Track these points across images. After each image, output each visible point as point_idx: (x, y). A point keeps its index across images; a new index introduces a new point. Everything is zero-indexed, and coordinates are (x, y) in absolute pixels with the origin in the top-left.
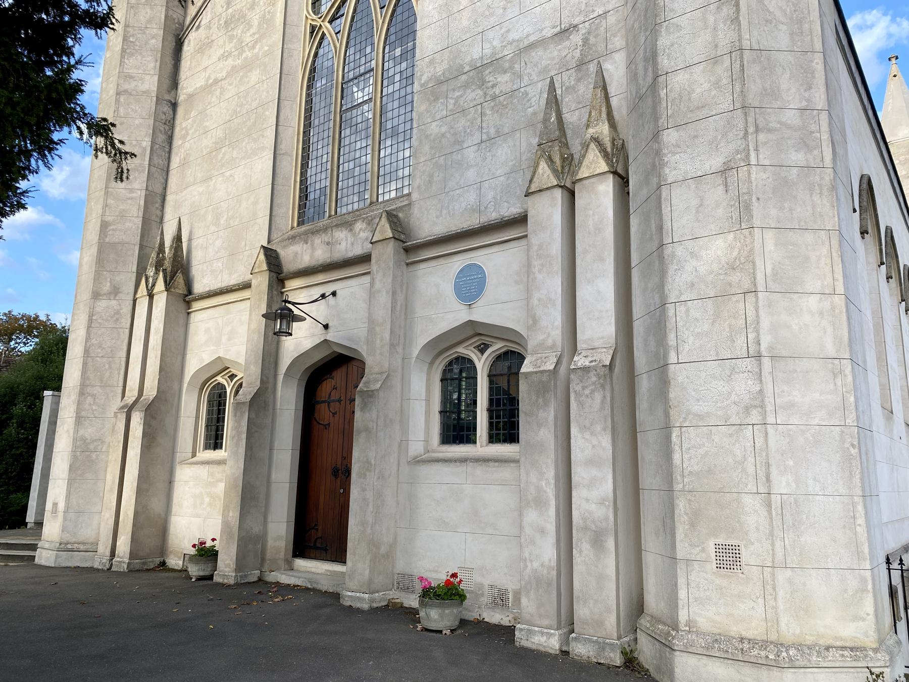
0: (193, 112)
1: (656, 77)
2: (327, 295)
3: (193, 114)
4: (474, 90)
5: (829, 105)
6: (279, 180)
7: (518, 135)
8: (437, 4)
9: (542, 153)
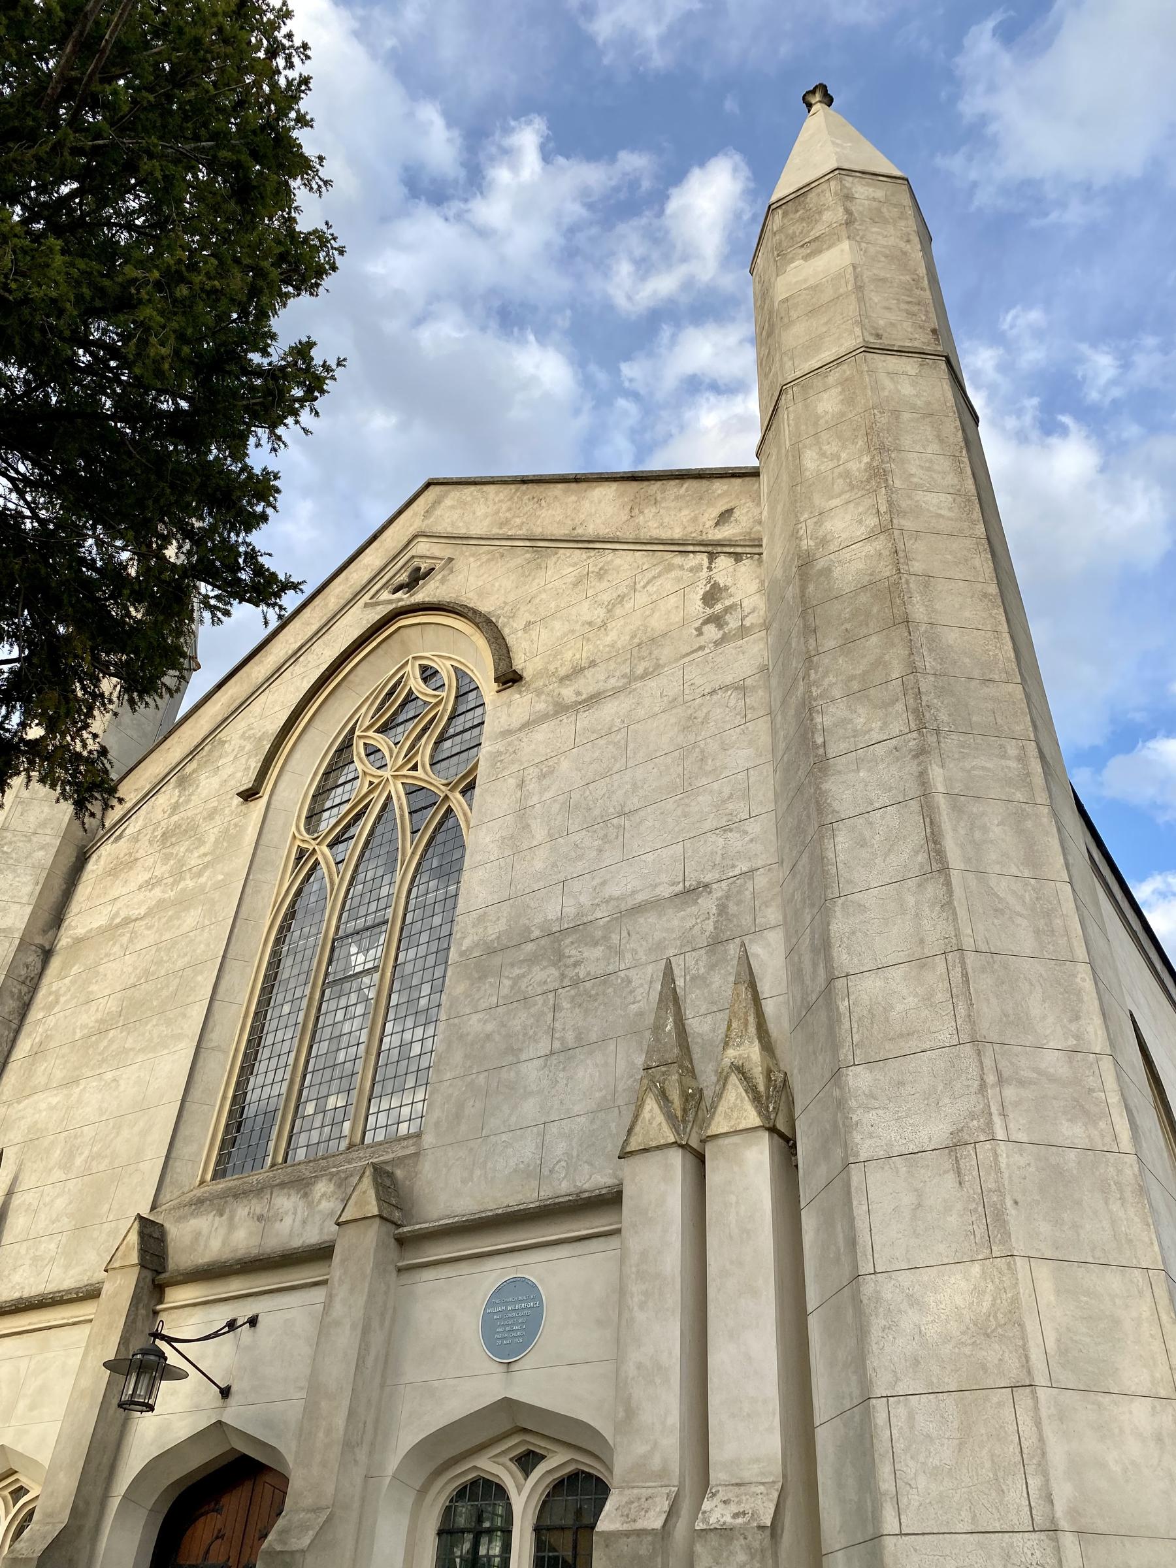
0: (76, 967)
1: (831, 980)
2: (239, 1323)
3: (75, 970)
4: (545, 968)
5: (1112, 1044)
6: (196, 1093)
7: (612, 1047)
8: (497, 836)
9: (651, 1084)
